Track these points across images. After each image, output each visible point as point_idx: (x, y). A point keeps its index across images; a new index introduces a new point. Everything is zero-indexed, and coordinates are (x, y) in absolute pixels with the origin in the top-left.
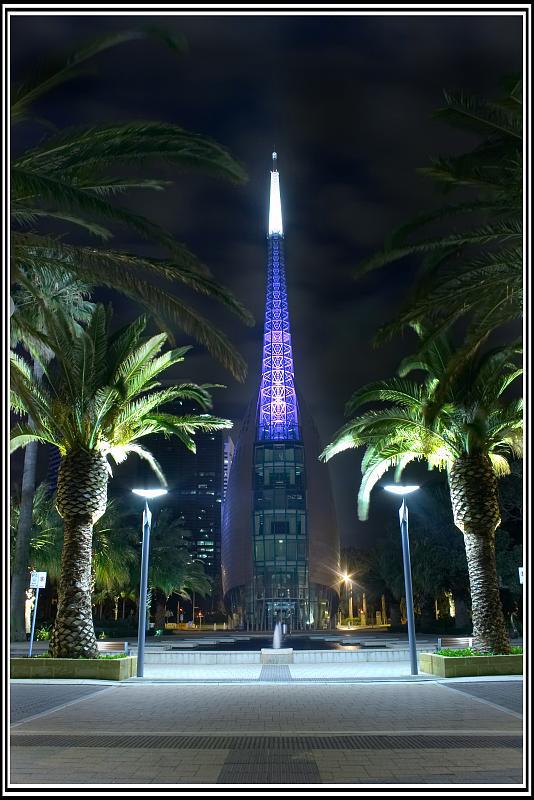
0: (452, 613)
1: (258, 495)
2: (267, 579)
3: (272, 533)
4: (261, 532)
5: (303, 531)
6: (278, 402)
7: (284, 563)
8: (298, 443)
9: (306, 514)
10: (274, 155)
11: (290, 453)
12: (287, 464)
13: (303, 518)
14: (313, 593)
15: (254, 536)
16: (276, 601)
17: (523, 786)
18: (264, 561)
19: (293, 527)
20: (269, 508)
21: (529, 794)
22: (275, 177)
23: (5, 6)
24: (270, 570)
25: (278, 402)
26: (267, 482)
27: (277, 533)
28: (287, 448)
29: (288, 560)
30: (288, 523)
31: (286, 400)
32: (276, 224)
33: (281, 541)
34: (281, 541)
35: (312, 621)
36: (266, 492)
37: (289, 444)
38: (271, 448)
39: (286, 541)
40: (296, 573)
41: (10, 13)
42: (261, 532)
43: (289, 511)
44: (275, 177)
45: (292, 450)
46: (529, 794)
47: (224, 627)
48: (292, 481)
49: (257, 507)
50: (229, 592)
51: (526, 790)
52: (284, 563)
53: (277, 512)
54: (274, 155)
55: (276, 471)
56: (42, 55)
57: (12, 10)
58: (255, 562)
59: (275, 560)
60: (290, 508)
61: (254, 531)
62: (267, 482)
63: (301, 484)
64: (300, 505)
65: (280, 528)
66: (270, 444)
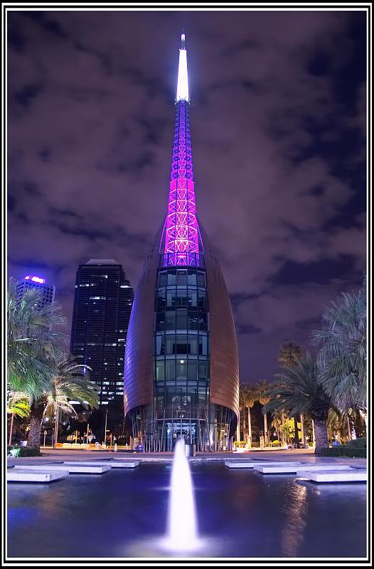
0: (41, 281)
1: (160, 317)
2: (167, 401)
3: (174, 353)
4: (162, 353)
5: (204, 352)
6: (182, 241)
7: (185, 384)
8: (199, 269)
9: (208, 336)
10: (183, 37)
11: (192, 278)
12: (189, 287)
13: (205, 339)
14: (213, 414)
15: (156, 355)
16: (175, 421)
17: (366, 560)
18: (165, 381)
19: (194, 348)
20: (172, 329)
21: (370, 565)
22: (183, 54)
23: (3, 4)
24: (170, 390)
25: (182, 241)
26: (169, 304)
27: (178, 353)
28: (190, 273)
29: (188, 380)
30: (189, 345)
31: (190, 237)
32: (183, 91)
33: (182, 362)
34: (182, 362)
35: (212, 442)
36: (169, 314)
37: (192, 270)
38: (174, 273)
39: (188, 362)
40: (197, 395)
41: (7, 9)
42: (162, 353)
43: (190, 332)
44: (183, 54)
45: (194, 276)
46: (370, 565)
47: (127, 447)
48: (194, 304)
49: (158, 329)
50: (131, 411)
51: (368, 562)
52: (185, 384)
53: (190, 332)
54: (183, 37)
55: (179, 296)
56: (25, 31)
57: (9, 7)
58: (156, 382)
59: (175, 380)
60: (192, 329)
61: (156, 352)
62: (169, 304)
63: (203, 306)
64: (203, 327)
65: (182, 349)
66: (173, 270)
